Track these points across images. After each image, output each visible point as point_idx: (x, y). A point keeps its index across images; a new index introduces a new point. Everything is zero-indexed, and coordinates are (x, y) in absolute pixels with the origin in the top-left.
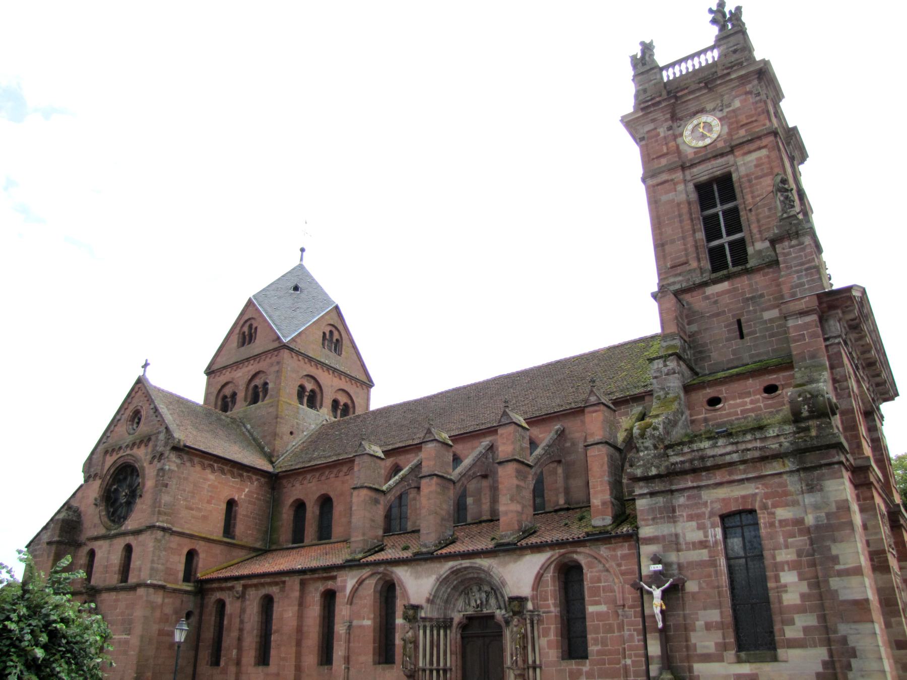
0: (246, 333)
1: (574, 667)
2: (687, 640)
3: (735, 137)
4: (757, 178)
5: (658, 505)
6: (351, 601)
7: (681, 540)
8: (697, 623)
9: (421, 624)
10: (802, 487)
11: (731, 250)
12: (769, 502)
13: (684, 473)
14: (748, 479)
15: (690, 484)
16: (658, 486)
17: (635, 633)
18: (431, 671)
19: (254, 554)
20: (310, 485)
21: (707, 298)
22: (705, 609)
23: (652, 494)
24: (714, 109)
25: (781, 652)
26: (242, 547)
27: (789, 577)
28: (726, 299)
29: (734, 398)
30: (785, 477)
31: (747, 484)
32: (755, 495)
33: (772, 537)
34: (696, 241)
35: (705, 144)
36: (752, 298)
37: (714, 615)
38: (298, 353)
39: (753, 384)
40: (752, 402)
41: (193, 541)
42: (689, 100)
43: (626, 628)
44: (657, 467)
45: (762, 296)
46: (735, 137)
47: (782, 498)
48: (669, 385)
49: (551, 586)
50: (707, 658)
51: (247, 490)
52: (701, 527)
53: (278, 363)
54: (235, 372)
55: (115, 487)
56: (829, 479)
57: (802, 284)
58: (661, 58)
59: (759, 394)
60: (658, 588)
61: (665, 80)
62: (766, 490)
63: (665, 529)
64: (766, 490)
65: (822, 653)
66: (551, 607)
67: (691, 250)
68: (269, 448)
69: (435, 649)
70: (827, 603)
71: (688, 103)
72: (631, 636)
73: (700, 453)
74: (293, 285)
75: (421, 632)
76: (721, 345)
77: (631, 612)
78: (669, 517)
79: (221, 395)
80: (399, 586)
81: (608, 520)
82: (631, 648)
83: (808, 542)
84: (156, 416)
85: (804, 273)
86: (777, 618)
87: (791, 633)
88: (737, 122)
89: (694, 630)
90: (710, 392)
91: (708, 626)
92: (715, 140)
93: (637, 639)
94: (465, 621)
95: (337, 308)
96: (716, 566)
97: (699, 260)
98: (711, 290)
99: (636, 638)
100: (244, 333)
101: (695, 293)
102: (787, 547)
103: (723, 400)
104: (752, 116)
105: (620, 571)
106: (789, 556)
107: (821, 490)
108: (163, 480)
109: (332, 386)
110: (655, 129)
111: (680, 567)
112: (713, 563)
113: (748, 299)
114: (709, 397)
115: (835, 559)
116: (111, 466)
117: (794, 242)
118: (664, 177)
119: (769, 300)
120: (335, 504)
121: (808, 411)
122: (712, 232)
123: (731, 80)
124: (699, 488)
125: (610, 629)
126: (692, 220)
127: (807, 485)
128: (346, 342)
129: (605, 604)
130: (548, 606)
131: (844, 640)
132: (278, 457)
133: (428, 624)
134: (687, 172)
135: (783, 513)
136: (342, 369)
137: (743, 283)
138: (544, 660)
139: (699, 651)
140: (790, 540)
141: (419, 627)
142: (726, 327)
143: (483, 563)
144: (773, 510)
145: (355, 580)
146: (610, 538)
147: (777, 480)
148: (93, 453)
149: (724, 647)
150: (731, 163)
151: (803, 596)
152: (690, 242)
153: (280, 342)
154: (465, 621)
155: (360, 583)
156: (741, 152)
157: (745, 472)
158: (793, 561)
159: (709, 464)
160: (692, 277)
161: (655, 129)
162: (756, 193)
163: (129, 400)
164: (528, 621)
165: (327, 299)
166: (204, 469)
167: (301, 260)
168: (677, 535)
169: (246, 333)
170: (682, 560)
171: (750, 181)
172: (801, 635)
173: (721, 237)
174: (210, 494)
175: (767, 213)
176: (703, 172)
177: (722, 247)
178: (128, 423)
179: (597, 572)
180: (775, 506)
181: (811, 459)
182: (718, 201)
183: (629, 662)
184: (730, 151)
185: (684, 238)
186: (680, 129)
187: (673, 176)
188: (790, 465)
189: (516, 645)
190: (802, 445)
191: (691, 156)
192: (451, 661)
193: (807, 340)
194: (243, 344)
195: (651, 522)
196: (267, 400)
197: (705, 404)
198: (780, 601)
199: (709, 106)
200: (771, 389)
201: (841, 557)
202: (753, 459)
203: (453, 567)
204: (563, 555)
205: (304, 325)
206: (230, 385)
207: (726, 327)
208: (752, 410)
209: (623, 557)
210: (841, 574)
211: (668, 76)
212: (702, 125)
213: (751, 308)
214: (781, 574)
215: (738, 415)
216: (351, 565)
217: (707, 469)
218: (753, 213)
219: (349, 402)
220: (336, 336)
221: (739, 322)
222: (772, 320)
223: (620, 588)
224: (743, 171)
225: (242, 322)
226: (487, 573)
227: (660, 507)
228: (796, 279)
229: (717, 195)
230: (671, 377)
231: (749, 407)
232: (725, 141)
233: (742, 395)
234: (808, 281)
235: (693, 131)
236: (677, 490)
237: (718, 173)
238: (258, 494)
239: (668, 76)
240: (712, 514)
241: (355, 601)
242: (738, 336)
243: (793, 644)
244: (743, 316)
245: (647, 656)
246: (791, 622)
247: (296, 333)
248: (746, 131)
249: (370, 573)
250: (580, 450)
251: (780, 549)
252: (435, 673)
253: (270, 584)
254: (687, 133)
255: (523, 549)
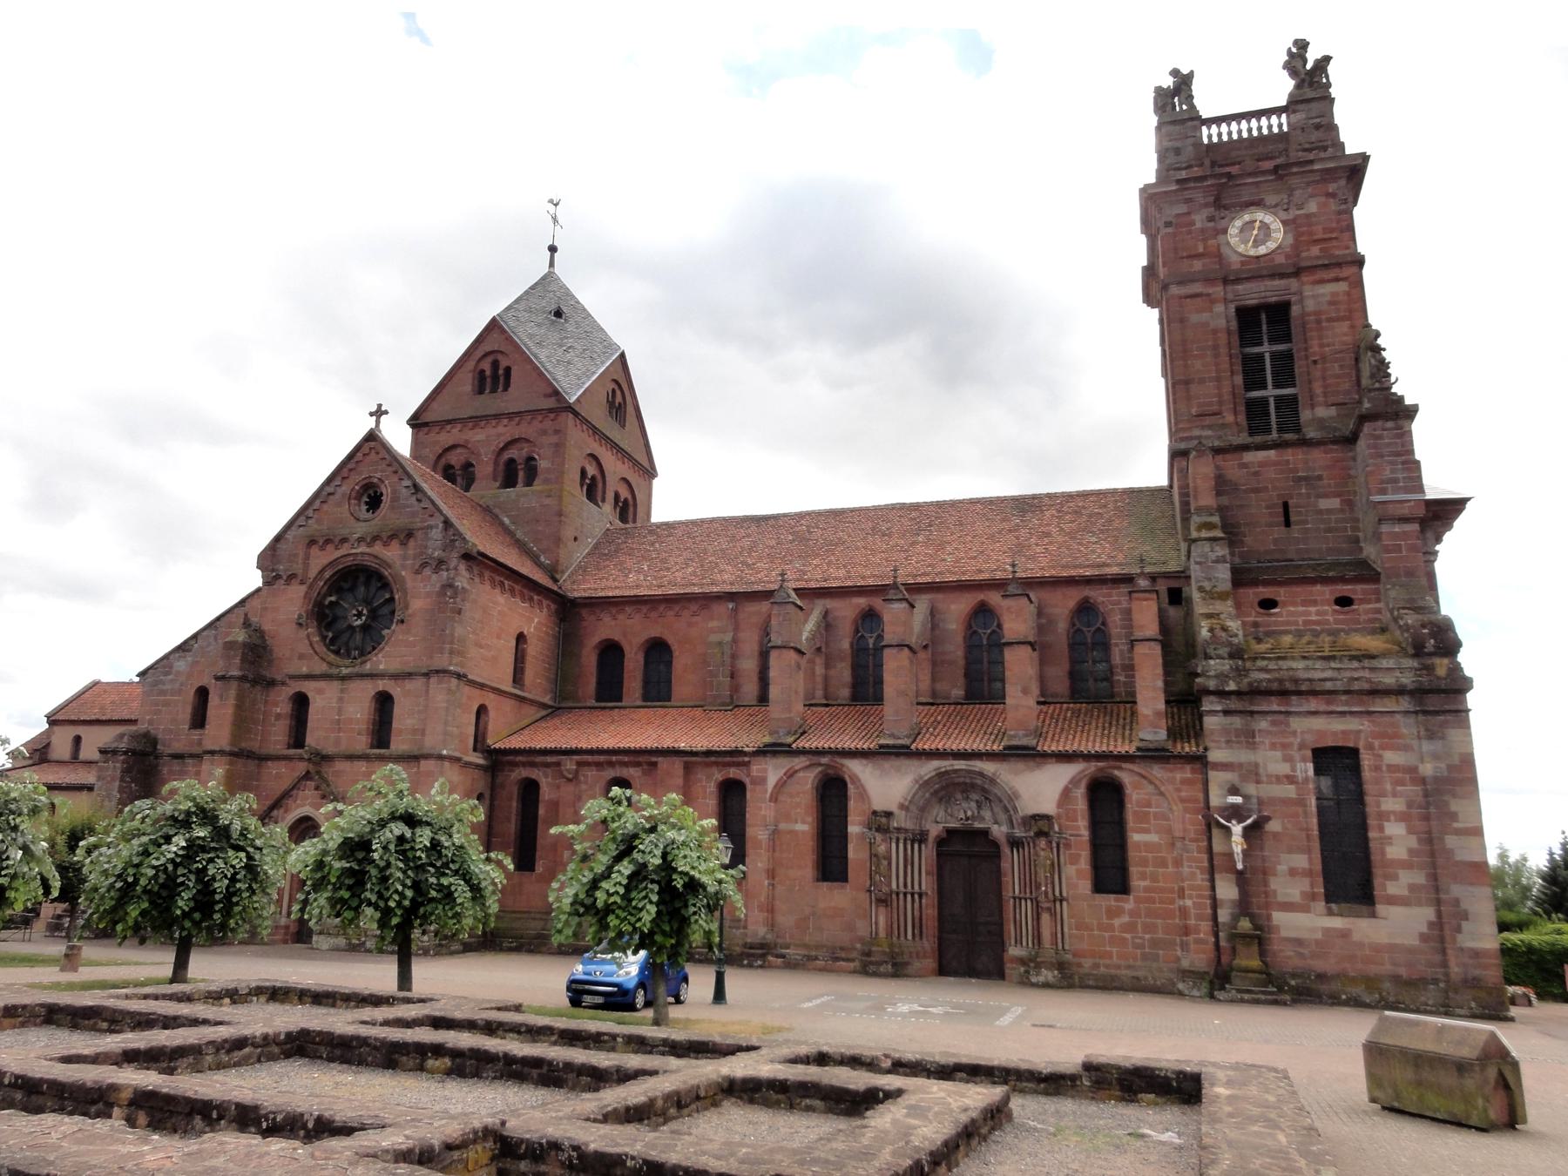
0: (488, 373)
1: (1113, 903)
2: (1266, 884)
3: (1304, 254)
4: (1330, 320)
5: (1234, 726)
6: (774, 798)
7: (1261, 771)
8: (1279, 867)
9: (894, 836)
10: (1419, 732)
11: (1277, 408)
12: (1376, 743)
13: (1269, 693)
14: (1351, 713)
15: (1275, 707)
16: (1234, 704)
17: (1198, 871)
18: (905, 894)
19: (544, 713)
20: (629, 622)
21: (1244, 466)
22: (1290, 851)
23: (1226, 713)
24: (1276, 206)
25: (1381, 908)
26: (532, 702)
27: (1395, 829)
28: (1271, 473)
29: (1294, 604)
30: (1398, 716)
31: (1348, 718)
32: (1359, 731)
33: (1378, 781)
34: (1233, 387)
35: (1257, 254)
36: (1306, 479)
37: (1301, 861)
38: (585, 421)
39: (1326, 592)
40: (1318, 613)
41: (483, 693)
42: (1245, 184)
43: (1185, 864)
44: (1238, 683)
45: (1320, 478)
46: (1304, 254)
47: (1391, 739)
48: (1216, 575)
49: (1081, 804)
50: (1288, 907)
51: (536, 620)
52: (1288, 759)
53: (557, 432)
54: (471, 432)
55: (333, 599)
56: (1453, 728)
57: (1395, 481)
58: (1207, 102)
59: (1329, 605)
60: (1239, 822)
61: (1206, 141)
62: (1373, 728)
63: (1243, 756)
64: (1373, 728)
65: (1428, 913)
66: (1081, 828)
67: (1227, 397)
68: (546, 558)
69: (909, 867)
70: (1440, 861)
71: (1243, 188)
72: (1193, 874)
73: (1291, 673)
74: (554, 307)
75: (894, 845)
76: (1258, 530)
77: (1193, 846)
78: (1248, 742)
79: (443, 461)
80: (853, 783)
81: (1162, 735)
82: (1192, 888)
83: (1421, 793)
84: (419, 500)
85: (1400, 466)
86: (1377, 872)
87: (1393, 889)
88: (1310, 233)
89: (1275, 875)
90: (1265, 592)
91: (1293, 872)
92: (1273, 251)
93: (1201, 879)
94: (945, 835)
95: (622, 355)
96: (1305, 806)
97: (1236, 414)
98: (1251, 457)
99: (1200, 877)
100: (483, 371)
101: (1228, 456)
102: (1395, 795)
103: (1280, 605)
104: (1332, 230)
105: (1180, 798)
106: (1397, 806)
107: (1443, 738)
108: (455, 603)
109: (615, 473)
110: (1189, 213)
111: (1261, 802)
112: (1301, 802)
113: (1300, 479)
114: (1262, 597)
115: (1454, 816)
116: (327, 566)
117: (1390, 424)
118: (1197, 288)
119: (1329, 486)
120: (676, 654)
121: (1434, 646)
122: (1254, 379)
123: (1312, 171)
124: (1288, 713)
125: (1164, 864)
126: (1231, 356)
127: (1427, 730)
128: (630, 409)
129: (1157, 832)
130: (1078, 828)
131: (1457, 902)
132: (563, 572)
133: (902, 836)
134: (1229, 288)
135: (1391, 757)
136: (625, 447)
137: (1293, 456)
138: (1071, 893)
139: (1280, 899)
140: (1399, 788)
141: (891, 839)
142: (1268, 507)
143: (988, 767)
144: (1381, 752)
145: (784, 771)
146: (1169, 757)
147: (1387, 719)
148: (278, 539)
149: (1313, 897)
150: (1293, 289)
151: (1411, 851)
152: (1226, 390)
153: (558, 401)
154: (945, 835)
155: (791, 774)
156: (1311, 278)
157: (1347, 703)
158: (1401, 812)
159: (1304, 688)
160: (1226, 435)
161: (1189, 213)
162: (1325, 341)
163: (351, 465)
164: (1054, 845)
165: (609, 345)
166: (494, 587)
167: (552, 264)
168: (1257, 765)
169: (488, 373)
170: (1262, 794)
171: (1319, 322)
172: (1406, 893)
173: (1265, 387)
174: (499, 624)
175: (1338, 371)
176: (1254, 293)
177: (1264, 401)
178: (353, 501)
179: (1146, 794)
180: (1383, 747)
181: (1433, 702)
182: (1265, 338)
183: (1189, 903)
184: (1293, 273)
185: (1218, 379)
186: (1223, 223)
187: (1210, 291)
188: (1405, 704)
189: (1045, 872)
190: (1426, 686)
191: (1236, 266)
192: (927, 884)
193: (1404, 553)
194: (481, 391)
195: (1224, 745)
196: (538, 486)
197: (1256, 605)
198: (1383, 853)
199: (1271, 199)
200: (1344, 602)
201: (1460, 815)
202: (1361, 690)
203: (939, 768)
204: (1101, 770)
205: (589, 377)
206: (459, 450)
207: (1268, 507)
208: (1315, 623)
209: (1184, 782)
210: (1459, 832)
211: (1210, 136)
212: (1257, 224)
213: (1303, 491)
214: (1386, 824)
215: (1298, 625)
216: (773, 750)
217: (1299, 693)
218: (1319, 366)
219: (630, 497)
220: (619, 399)
221: (1286, 506)
222: (1329, 511)
223: (1185, 822)
224: (1310, 305)
225: (479, 353)
226: (992, 781)
227: (1236, 730)
228: (1388, 472)
229: (1264, 327)
230: (1220, 566)
231: (1314, 618)
232: (1287, 257)
233: (1305, 603)
234: (1404, 478)
235: (1242, 230)
236: (1258, 712)
237: (1274, 299)
238: (547, 627)
239: (1210, 136)
240: (1302, 747)
241: (781, 798)
242: (1283, 524)
243: (1392, 901)
244: (1292, 498)
245: (1214, 899)
246: (1395, 878)
247: (582, 390)
248: (1321, 249)
249: (808, 763)
250: (1060, 631)
251: (1385, 796)
252: (909, 897)
253: (626, 764)
254: (1233, 230)
255: (1045, 756)
